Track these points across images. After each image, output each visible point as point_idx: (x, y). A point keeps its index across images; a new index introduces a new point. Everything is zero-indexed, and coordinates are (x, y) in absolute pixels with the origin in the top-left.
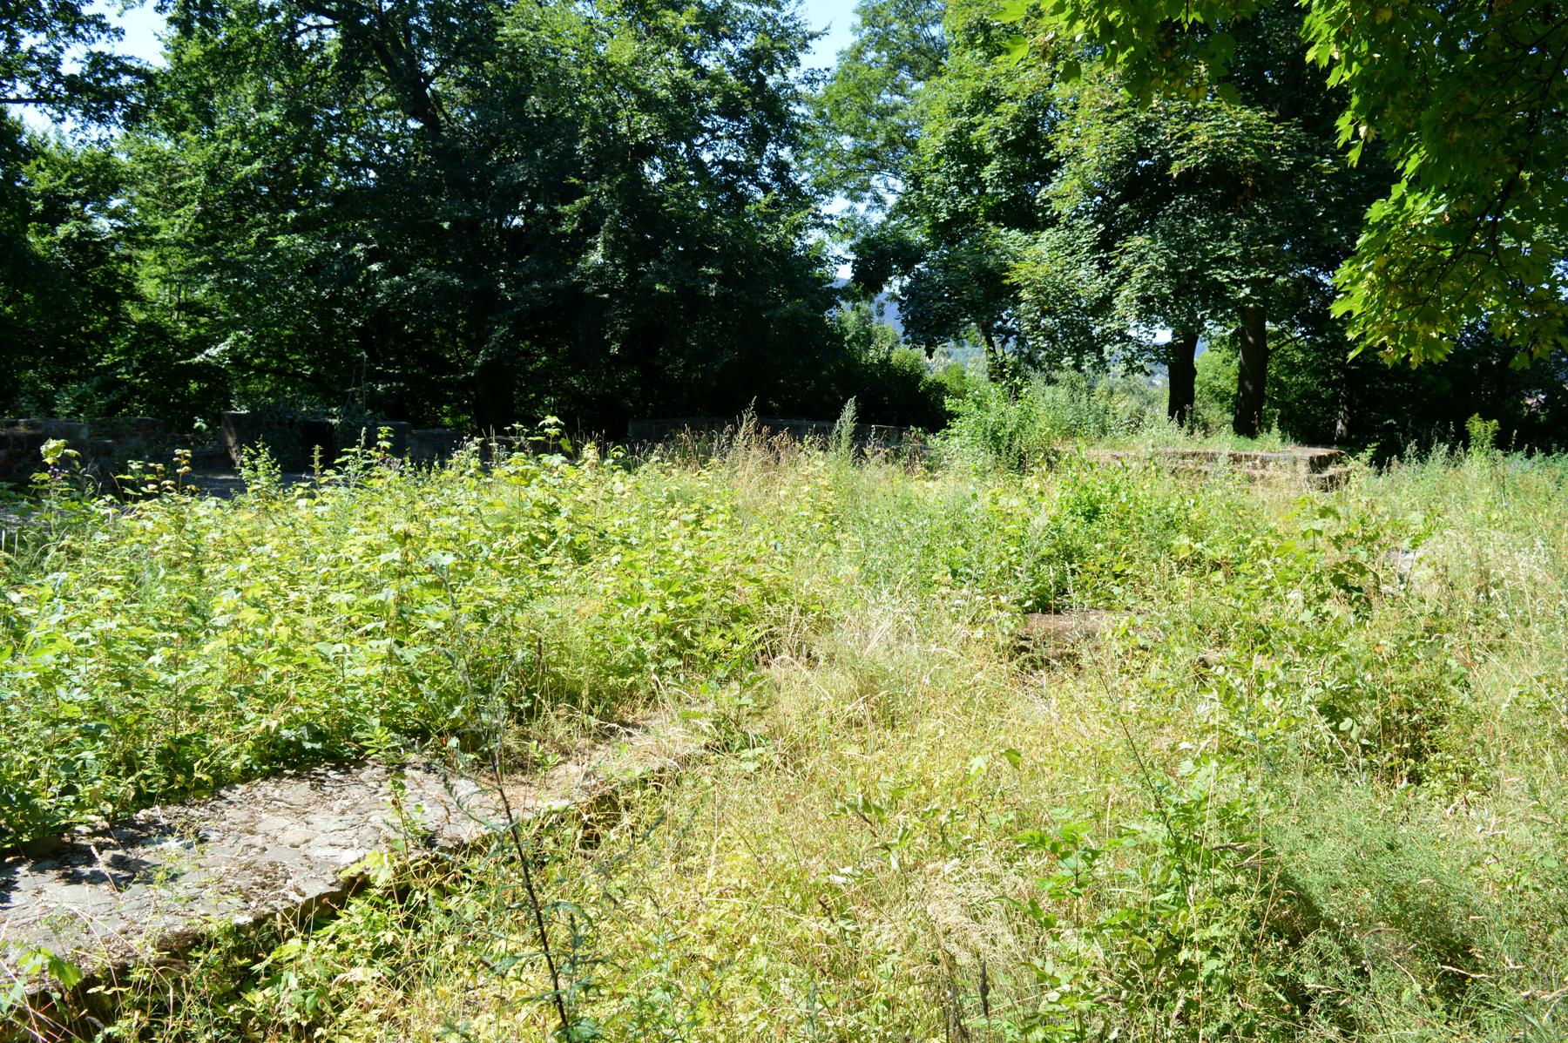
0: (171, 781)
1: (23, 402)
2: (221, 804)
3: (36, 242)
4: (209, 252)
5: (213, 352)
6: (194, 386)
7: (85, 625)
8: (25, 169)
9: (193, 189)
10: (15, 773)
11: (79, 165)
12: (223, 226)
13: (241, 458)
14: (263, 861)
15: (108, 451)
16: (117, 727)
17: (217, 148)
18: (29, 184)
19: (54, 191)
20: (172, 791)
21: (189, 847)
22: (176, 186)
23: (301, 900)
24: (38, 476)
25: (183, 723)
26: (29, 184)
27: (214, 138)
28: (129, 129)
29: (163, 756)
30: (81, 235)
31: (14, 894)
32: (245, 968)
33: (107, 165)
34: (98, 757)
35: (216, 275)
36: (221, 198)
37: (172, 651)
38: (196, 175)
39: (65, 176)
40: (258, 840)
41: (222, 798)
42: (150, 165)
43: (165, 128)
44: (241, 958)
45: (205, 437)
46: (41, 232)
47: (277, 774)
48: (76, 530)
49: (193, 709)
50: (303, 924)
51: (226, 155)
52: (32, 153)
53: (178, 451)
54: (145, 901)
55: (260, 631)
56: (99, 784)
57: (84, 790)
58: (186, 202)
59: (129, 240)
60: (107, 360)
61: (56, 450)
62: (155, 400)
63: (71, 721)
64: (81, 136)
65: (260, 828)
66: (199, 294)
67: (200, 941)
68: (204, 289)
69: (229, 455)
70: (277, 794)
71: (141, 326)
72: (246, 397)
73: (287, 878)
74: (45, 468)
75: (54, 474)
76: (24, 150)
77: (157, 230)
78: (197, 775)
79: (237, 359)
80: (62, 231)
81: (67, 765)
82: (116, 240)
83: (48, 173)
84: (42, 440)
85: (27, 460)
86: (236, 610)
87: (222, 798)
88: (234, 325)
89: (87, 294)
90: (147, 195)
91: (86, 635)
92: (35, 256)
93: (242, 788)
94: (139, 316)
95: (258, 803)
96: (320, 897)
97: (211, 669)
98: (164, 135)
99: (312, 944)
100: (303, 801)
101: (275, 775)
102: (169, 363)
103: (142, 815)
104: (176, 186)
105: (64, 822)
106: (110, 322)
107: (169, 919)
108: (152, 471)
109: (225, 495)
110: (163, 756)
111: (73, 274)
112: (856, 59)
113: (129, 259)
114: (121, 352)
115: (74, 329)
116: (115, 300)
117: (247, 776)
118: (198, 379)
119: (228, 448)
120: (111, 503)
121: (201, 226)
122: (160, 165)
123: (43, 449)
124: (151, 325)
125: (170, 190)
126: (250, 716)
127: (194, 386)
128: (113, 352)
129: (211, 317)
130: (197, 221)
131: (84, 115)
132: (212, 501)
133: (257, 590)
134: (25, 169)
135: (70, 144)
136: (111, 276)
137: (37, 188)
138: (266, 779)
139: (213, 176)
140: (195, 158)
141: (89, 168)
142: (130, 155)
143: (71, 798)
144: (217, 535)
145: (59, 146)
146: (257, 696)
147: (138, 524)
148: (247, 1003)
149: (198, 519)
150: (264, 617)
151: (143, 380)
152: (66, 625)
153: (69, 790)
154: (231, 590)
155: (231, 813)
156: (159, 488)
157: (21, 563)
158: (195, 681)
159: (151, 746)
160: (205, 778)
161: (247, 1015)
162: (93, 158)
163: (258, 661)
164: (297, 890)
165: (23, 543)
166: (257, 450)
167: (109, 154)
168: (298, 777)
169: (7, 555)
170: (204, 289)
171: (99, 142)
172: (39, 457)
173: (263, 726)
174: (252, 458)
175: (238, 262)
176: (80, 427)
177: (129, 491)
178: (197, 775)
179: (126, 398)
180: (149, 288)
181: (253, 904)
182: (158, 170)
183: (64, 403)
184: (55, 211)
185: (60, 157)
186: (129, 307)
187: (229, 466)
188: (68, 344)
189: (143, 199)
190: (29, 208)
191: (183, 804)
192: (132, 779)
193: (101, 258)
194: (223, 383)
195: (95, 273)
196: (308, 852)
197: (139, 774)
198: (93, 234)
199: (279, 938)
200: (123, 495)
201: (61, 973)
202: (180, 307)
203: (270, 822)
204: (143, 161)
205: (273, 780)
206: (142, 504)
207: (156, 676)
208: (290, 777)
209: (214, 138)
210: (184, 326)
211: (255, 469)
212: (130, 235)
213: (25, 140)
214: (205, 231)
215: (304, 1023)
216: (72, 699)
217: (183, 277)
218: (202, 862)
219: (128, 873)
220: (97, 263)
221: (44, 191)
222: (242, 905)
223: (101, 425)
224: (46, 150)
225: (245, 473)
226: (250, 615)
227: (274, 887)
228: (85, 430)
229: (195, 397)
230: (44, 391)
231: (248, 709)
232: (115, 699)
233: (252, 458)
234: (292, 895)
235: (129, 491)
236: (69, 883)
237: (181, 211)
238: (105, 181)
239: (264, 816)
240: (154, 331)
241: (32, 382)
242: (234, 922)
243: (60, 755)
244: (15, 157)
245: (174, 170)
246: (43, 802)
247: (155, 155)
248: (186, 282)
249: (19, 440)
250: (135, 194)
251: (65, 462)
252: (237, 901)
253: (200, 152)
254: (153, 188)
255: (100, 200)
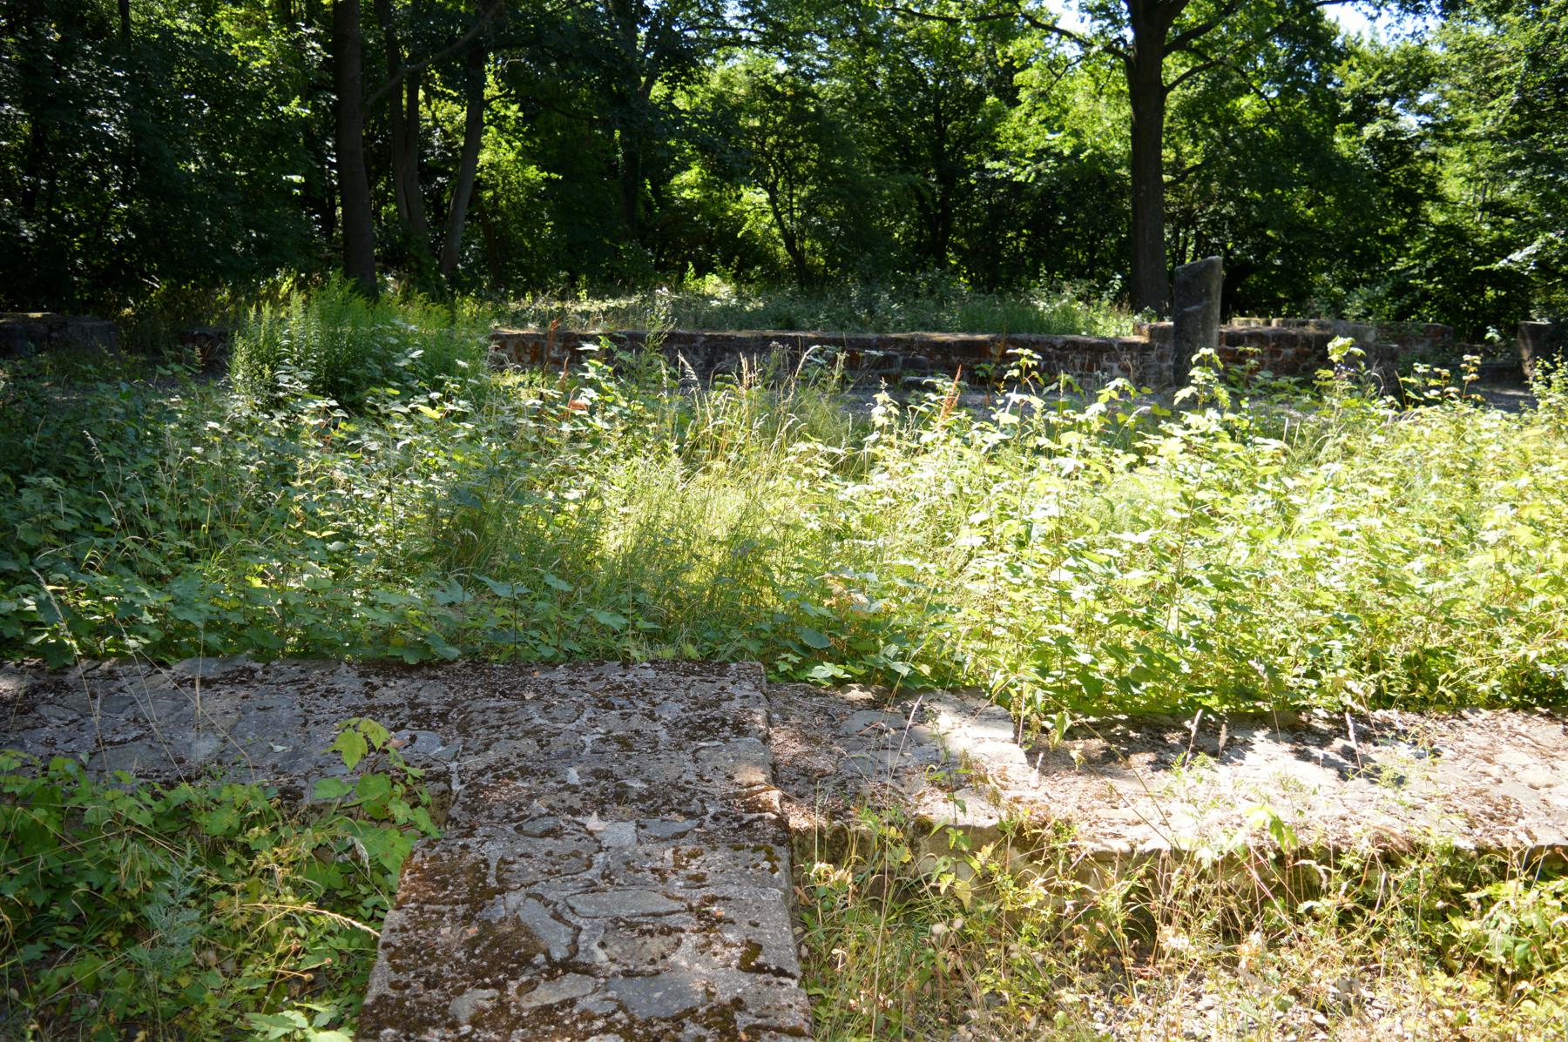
0: (1413, 688)
1: (1314, 302)
2: (1462, 724)
3: (1342, 143)
4: (1523, 145)
5: (1517, 256)
6: (1490, 293)
7: (1351, 517)
8: (1337, 70)
9: (1511, 77)
10: (1267, 647)
11: (1391, 62)
12: (1541, 116)
13: (1534, 372)
14: (1496, 792)
15: (1393, 357)
16: (1368, 624)
17: (1543, 29)
18: (1340, 85)
19: (1363, 91)
20: (1413, 699)
21: (1419, 757)
22: (1492, 75)
23: (1530, 844)
24: (1324, 373)
25: (1434, 635)
26: (1340, 85)
27: (1539, 16)
28: (1446, 18)
29: (1408, 663)
30: (1388, 134)
31: (1248, 754)
32: (1455, 893)
33: (1420, 58)
34: (1345, 649)
35: (1529, 170)
36: (1542, 84)
37: (1433, 560)
38: (1515, 61)
39: (1376, 74)
40: (1495, 771)
41: (1462, 718)
42: (1465, 55)
43: (1486, 12)
44: (1454, 880)
45: (1496, 349)
46: (1348, 133)
47: (1528, 708)
48: (1351, 428)
49: (1448, 621)
50: (1529, 865)
51: (1552, 36)
52: (1342, 55)
53: (1467, 357)
54: (1367, 796)
55: (1532, 553)
56: (1342, 673)
57: (1326, 676)
58: (1501, 92)
59: (1436, 136)
60: (1402, 263)
61: (1342, 347)
62: (1447, 308)
63: (1324, 609)
64: (1395, 30)
65: (1499, 758)
66: (1506, 194)
67: (1419, 850)
68: (1514, 185)
69: (1521, 369)
70: (1523, 729)
71: (1440, 229)
72: (1548, 307)
73: (1519, 817)
74: (1331, 365)
75: (1340, 371)
76: (1338, 52)
77: (1466, 124)
78: (1441, 688)
79: (1544, 265)
80: (1368, 131)
81: (1314, 648)
82: (1422, 138)
83: (1359, 73)
84: (1330, 338)
85: (1313, 360)
86: (1509, 527)
87: (1462, 718)
88: (1545, 227)
89: (1389, 194)
90: (1460, 87)
91: (1351, 527)
92: (1339, 157)
93: (1486, 714)
94: (1439, 218)
95: (1501, 733)
96: (1552, 847)
97: (1471, 584)
98: (1484, 20)
99: (1534, 893)
100: (1552, 744)
101: (1525, 709)
102: (1467, 269)
103: (1379, 714)
104: (1492, 75)
105: (1303, 703)
106: (1409, 224)
107: (1390, 820)
108: (1438, 376)
109: (1512, 407)
110: (1408, 663)
111: (1377, 175)
112: (1109, 756)
113: (1434, 157)
114: (1417, 256)
115: (1370, 231)
116: (1416, 201)
117: (1493, 702)
118: (1495, 287)
119: (1520, 363)
120: (1391, 406)
121: (1516, 117)
122: (1476, 54)
123: (1330, 346)
124: (1452, 226)
125: (1484, 81)
126: (1507, 640)
127: (1490, 293)
128: (1408, 256)
129: (1518, 218)
130: (1512, 112)
131: (1400, 7)
132: (1496, 414)
133: (1534, 511)
134: (1337, 70)
135: (1383, 41)
136: (1414, 176)
137: (1346, 90)
138: (1514, 711)
139: (1536, 60)
140: (1518, 41)
141: (1401, 64)
142: (1445, 45)
143: (1312, 683)
144: (1499, 449)
145: (1373, 43)
146: (1519, 621)
147: (1416, 430)
148: (1452, 927)
149: (1478, 431)
150: (1539, 540)
151: (1435, 286)
152: (1334, 515)
153: (1312, 674)
154: (1506, 505)
155: (1471, 736)
156: (1442, 394)
157: (1298, 455)
158: (1452, 595)
159: (1396, 652)
160: (1449, 693)
161: (1449, 940)
162: (1405, 53)
163: (1527, 585)
164: (1529, 833)
165: (1302, 437)
166: (1554, 364)
167: (1423, 46)
168: (1550, 716)
169: (1286, 446)
170: (1514, 185)
171: (1414, 34)
172: (1326, 354)
173: (1520, 654)
174: (1547, 372)
175: (1556, 155)
176: (1368, 330)
177: (1411, 394)
178: (1441, 688)
179: (1417, 304)
180: (1452, 187)
181: (1478, 832)
182: (1474, 59)
183: (1355, 305)
184: (1364, 110)
185: (1372, 55)
186: (1429, 208)
187: (1520, 381)
188: (1364, 247)
189: (1455, 93)
190: (1337, 109)
191: (1421, 714)
192: (1374, 676)
193: (1405, 157)
194: (1522, 291)
195: (1398, 173)
196: (1548, 797)
197: (1382, 672)
198: (1400, 133)
199: (1502, 873)
200: (1404, 400)
201: (1280, 834)
202: (1485, 207)
203: (1510, 755)
204: (1458, 51)
205: (1522, 714)
206: (1422, 409)
207: (1416, 582)
208: (1542, 715)
209: (1539, 16)
210: (1486, 227)
211: (1549, 384)
212: (1437, 132)
213: (1339, 41)
214: (1520, 123)
215: (1509, 971)
216: (1335, 582)
217: (1491, 174)
218: (1431, 775)
219: (1348, 767)
220: (1400, 163)
221: (1354, 92)
222: (1466, 829)
223: (1389, 329)
224: (1359, 49)
225: (1537, 388)
226: (1524, 534)
227: (1502, 821)
228: (1372, 333)
229: (1490, 306)
230: (1335, 295)
231: (1508, 632)
232: (1369, 594)
233: (1547, 372)
234: (1522, 836)
235: (1411, 394)
236: (1298, 758)
237: (1495, 103)
238: (1416, 75)
239: (1505, 747)
240: (1454, 234)
241: (1325, 285)
242: (1454, 843)
243: (1311, 638)
244: (1328, 59)
245: (1491, 58)
246: (1288, 679)
247: (1472, 43)
248: (1494, 180)
249: (1307, 340)
250: (1447, 87)
251: (1350, 360)
252: (1460, 823)
253: (1523, 35)
254: (1466, 79)
255: (1410, 96)
